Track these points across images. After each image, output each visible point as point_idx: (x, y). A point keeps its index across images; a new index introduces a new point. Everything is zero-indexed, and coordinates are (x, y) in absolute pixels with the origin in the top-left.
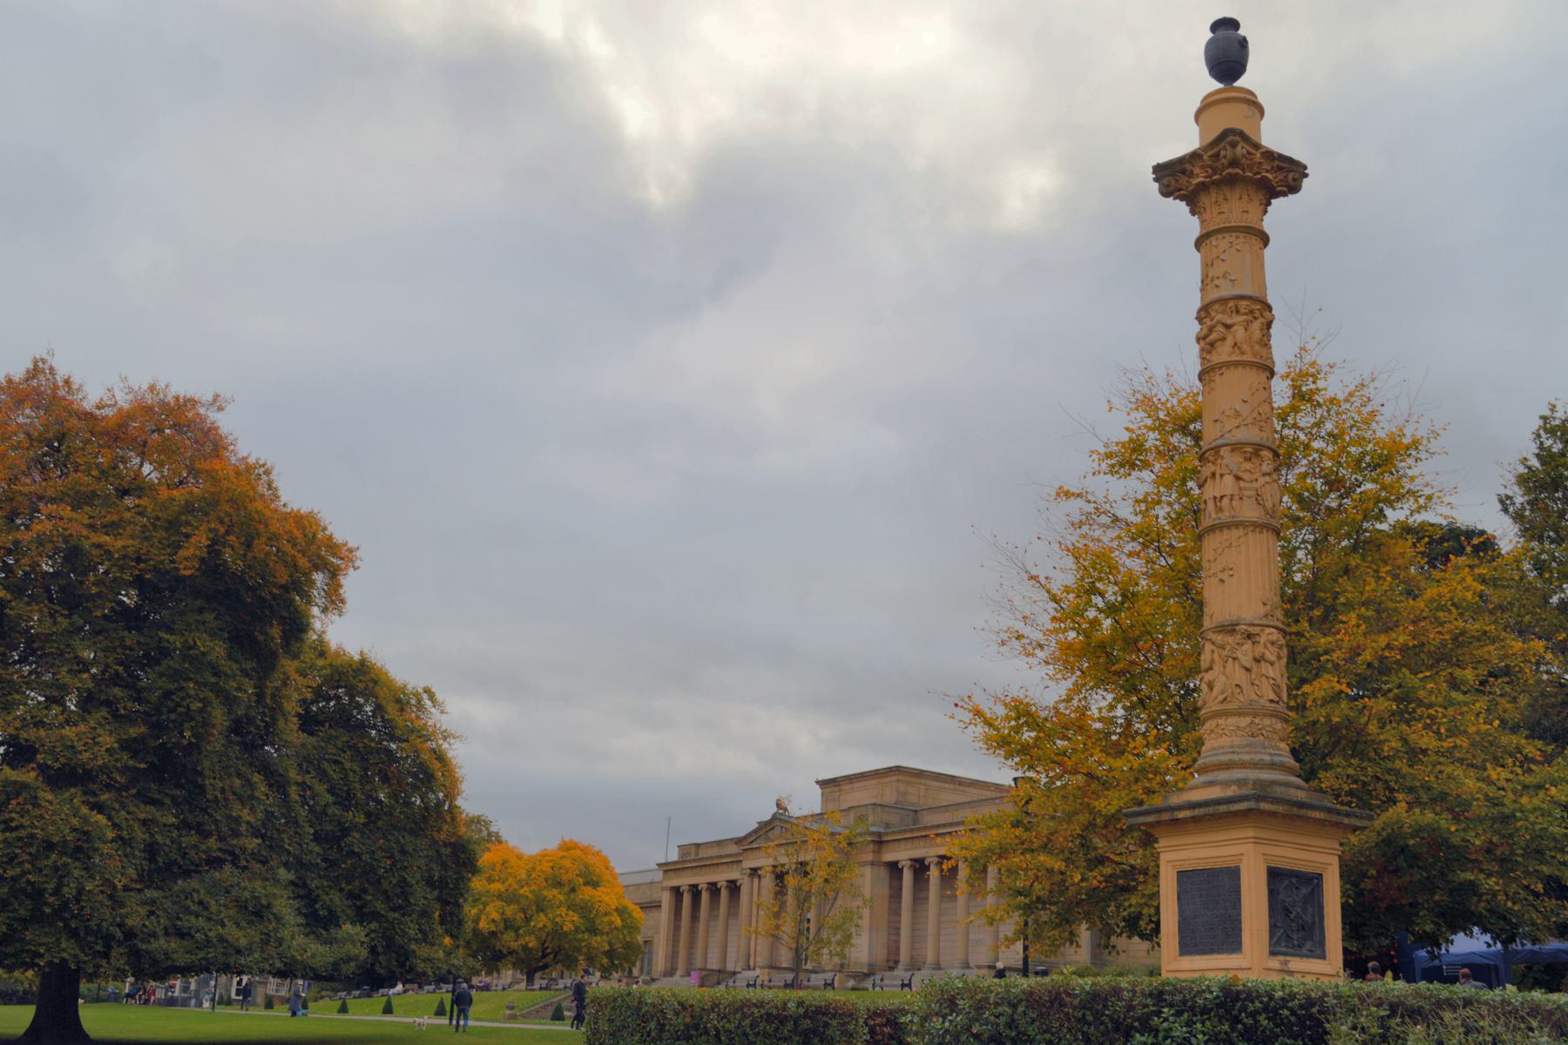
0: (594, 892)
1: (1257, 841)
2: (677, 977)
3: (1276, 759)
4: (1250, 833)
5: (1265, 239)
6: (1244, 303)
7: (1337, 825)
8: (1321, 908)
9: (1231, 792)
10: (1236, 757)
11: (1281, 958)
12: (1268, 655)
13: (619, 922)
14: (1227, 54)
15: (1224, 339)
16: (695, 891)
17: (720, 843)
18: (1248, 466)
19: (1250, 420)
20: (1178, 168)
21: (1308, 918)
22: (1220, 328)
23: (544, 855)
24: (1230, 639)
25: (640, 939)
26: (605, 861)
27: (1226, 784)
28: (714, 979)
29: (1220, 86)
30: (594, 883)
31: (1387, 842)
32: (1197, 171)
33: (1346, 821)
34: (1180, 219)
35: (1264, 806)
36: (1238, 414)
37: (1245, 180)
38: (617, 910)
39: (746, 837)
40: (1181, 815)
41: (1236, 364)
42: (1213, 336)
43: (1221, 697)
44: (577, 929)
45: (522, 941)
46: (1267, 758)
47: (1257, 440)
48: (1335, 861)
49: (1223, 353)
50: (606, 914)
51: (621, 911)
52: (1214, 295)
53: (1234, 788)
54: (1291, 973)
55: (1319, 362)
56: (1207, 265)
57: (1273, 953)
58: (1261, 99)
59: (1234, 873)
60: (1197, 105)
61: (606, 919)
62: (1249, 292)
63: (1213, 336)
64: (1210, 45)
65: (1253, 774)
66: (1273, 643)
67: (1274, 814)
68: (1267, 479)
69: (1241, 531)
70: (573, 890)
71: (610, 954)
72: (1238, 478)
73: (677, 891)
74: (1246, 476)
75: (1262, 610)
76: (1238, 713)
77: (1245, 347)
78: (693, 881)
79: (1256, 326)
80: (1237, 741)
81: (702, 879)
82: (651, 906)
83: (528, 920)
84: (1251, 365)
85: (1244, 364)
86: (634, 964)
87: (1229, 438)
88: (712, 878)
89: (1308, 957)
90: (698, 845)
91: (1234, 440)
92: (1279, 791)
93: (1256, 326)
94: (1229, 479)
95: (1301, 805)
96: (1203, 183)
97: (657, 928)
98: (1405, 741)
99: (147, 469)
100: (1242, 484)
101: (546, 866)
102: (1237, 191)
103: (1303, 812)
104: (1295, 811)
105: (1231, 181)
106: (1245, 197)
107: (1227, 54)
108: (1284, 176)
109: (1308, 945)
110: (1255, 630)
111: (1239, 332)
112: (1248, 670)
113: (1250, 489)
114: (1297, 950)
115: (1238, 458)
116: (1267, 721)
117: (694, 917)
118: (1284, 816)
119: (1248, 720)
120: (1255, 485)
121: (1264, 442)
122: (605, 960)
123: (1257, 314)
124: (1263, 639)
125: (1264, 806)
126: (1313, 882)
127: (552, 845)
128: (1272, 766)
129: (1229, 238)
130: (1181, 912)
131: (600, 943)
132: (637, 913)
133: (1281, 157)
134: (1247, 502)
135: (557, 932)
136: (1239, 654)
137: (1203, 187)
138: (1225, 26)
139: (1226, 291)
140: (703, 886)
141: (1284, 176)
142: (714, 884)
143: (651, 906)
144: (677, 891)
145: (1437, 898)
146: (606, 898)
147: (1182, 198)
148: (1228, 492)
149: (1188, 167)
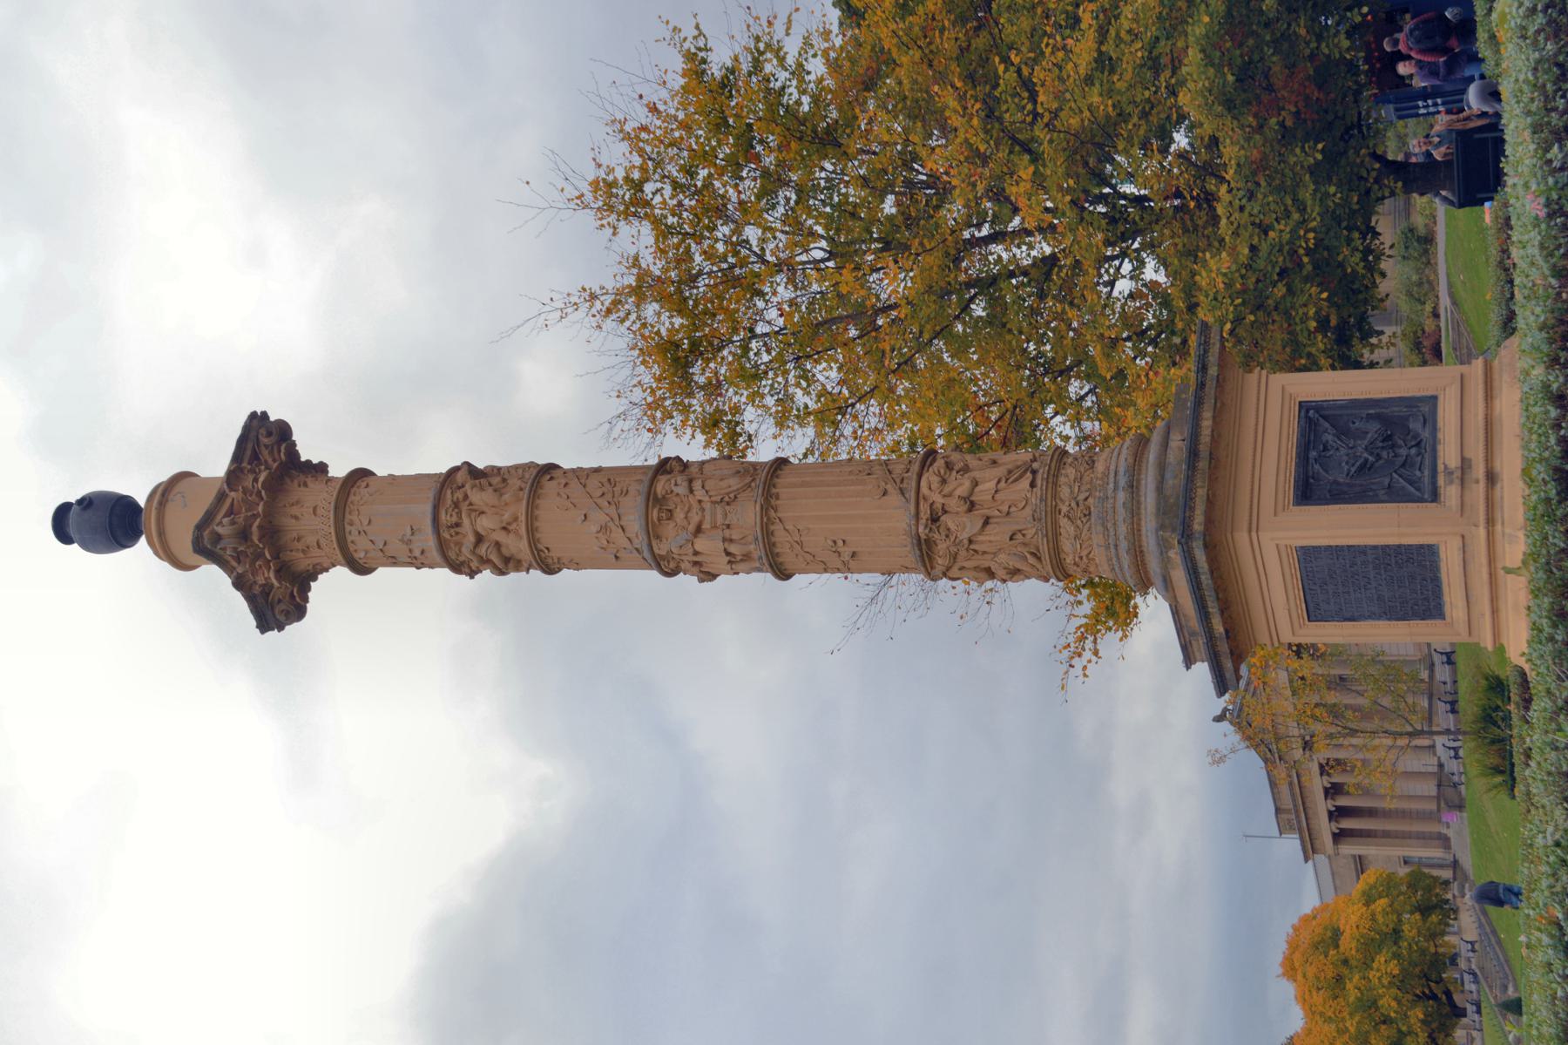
0: (1347, 934)
1: (1254, 527)
2: (1450, 833)
3: (1122, 481)
4: (1242, 538)
5: (360, 475)
6: (443, 516)
7: (1220, 382)
8: (1355, 404)
9: (1175, 555)
10: (1124, 545)
11: (1441, 481)
12: (963, 490)
13: (1383, 902)
14: (101, 522)
15: (498, 545)
16: (1338, 813)
17: (1273, 785)
18: (679, 515)
19: (612, 511)
20: (260, 600)
21: (1374, 428)
22: (482, 550)
23: (1303, 1000)
24: (942, 547)
25: (1403, 871)
26: (1306, 920)
27: (1166, 563)
28: (1449, 791)
29: (143, 539)
30: (1337, 934)
31: (1229, 105)
32: (261, 580)
33: (1213, 371)
34: (333, 589)
35: (1198, 525)
36: (604, 529)
37: (269, 514)
38: (1367, 904)
39: (1266, 761)
40: (1219, 627)
41: (532, 531)
42: (494, 558)
43: (1031, 560)
44: (1396, 956)
45: (1417, 1027)
46: (1122, 496)
47: (641, 500)
49: (517, 545)
50: (1373, 919)
51: (1368, 899)
52: (435, 554)
53: (1172, 554)
54: (1465, 464)
55: (591, 178)
56: (394, 562)
57: (1435, 497)
58: (164, 476)
59: (1308, 555)
60: (166, 565)
61: (1380, 919)
62: (428, 508)
63: (494, 558)
64: (87, 546)
65: (1149, 523)
66: (944, 481)
67: (1210, 502)
68: (697, 485)
69: (777, 527)
70: (1346, 962)
71: (1425, 910)
72: (698, 530)
73: (1339, 836)
74: (695, 519)
75: (894, 498)
76: (1055, 536)
77: (507, 517)
78: (1324, 817)
79: (477, 497)
80: (1097, 539)
81: (1321, 807)
82: (1361, 864)
83: (1386, 1021)
84: (532, 506)
85: (531, 518)
86: (1436, 879)
87: (641, 541)
88: (1319, 794)
89: (1435, 429)
90: (1278, 811)
91: (643, 537)
92: (1174, 482)
93: (477, 497)
94: (701, 544)
95: (1193, 454)
96: (278, 572)
97: (1385, 857)
98: (1089, 80)
99: (938, 431)
100: (706, 526)
101: (1318, 998)
102: (288, 522)
104: (1203, 464)
105: (272, 533)
106: (295, 510)
107: (101, 522)
108: (265, 442)
109: (1415, 425)
110: (925, 513)
111: (484, 524)
112: (987, 522)
113: (714, 515)
114: (1426, 447)
115: (669, 529)
116: (1065, 492)
117: (1371, 813)
118: (1213, 480)
119: (1064, 522)
120: (707, 506)
121: (644, 488)
122: (1434, 918)
123: (459, 495)
124: (938, 500)
125: (1198, 525)
126: (1314, 417)
127: (1288, 989)
128: (1133, 487)
129: (352, 536)
130: (1372, 616)
131: (1411, 924)
132: (1370, 877)
133: (237, 457)
134: (732, 519)
135: (1401, 982)
136: (964, 536)
137: (284, 570)
138: (65, 523)
139: (431, 543)
140: (1330, 805)
141: (265, 442)
142: (1327, 791)
143: (1361, 864)
144: (1339, 836)
145: (1303, 32)
146: (1352, 920)
147: (305, 590)
148: (721, 546)
149: (257, 590)
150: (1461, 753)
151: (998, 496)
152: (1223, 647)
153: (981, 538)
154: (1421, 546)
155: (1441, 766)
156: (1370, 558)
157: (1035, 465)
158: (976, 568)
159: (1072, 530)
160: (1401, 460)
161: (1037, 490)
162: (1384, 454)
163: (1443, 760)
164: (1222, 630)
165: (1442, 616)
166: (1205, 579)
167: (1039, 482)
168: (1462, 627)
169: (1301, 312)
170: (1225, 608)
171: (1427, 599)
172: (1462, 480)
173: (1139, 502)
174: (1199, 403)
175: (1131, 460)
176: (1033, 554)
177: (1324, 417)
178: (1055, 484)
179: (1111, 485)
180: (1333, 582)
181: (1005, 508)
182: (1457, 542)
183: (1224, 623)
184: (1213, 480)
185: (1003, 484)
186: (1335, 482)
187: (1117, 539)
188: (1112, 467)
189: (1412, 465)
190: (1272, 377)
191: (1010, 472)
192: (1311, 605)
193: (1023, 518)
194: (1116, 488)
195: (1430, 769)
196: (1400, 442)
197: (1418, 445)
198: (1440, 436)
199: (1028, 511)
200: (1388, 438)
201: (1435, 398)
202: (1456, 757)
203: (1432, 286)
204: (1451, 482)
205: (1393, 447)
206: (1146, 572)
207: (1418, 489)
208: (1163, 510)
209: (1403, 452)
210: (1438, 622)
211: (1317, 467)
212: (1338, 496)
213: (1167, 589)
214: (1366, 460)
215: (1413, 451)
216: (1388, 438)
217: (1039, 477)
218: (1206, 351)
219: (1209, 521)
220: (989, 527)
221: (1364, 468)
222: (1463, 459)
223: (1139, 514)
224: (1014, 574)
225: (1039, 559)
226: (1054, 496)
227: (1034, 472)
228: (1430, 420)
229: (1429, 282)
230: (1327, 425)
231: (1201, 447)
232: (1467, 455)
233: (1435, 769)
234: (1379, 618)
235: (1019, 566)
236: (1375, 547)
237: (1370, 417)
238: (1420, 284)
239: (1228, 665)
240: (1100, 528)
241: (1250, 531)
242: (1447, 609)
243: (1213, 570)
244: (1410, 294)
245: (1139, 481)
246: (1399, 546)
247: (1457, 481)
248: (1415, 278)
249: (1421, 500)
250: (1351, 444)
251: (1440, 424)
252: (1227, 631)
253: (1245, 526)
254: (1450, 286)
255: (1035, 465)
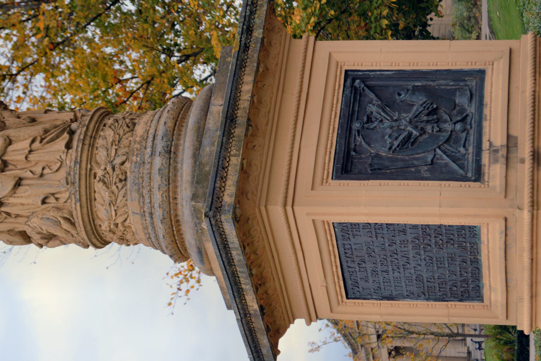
1: (290, 201)
3: (160, 145)
4: (276, 211)
7: (265, 46)
10: (158, 213)
11: (485, 158)
21: (419, 101)
33: (258, 33)
35: (228, 197)
40: (253, 305)
43: (66, 225)
46: (158, 161)
48: (326, 47)
54: (511, 142)
57: (478, 175)
59: (345, 232)
65: (185, 191)
67: (244, 172)
80: (133, 206)
89: (481, 105)
92: (210, 149)
95: (230, 119)
103: (241, 115)
104: (239, 131)
109: (461, 100)
112: (19, 183)
114: (471, 123)
116: (101, 155)
118: (249, 146)
119: (98, 186)
125: (228, 197)
126: (358, 86)
128: (171, 152)
150: (483, 346)
151: (31, 157)
152: (259, 324)
153: (12, 200)
154: (463, 227)
155: (469, 353)
156: (410, 237)
157: (74, 126)
158: (10, 232)
159: (106, 195)
160: (446, 135)
161: (72, 152)
162: (429, 129)
163: (471, 349)
164: (256, 307)
165: (479, 297)
166: (237, 255)
167: (75, 143)
168: (500, 311)
169: (375, 12)
170: (259, 284)
171: (465, 281)
172: (507, 159)
173: (175, 169)
174: (240, 65)
175: (170, 124)
176: (65, 219)
177: (369, 88)
178: (92, 146)
179: (149, 150)
180: (368, 261)
181: (38, 170)
182: (498, 227)
183: (259, 299)
184: (249, 146)
185: (37, 144)
186: (377, 156)
187: (152, 207)
188: (152, 131)
189: (457, 141)
190: (319, 43)
191: (46, 131)
192: (349, 283)
193: (56, 181)
194: (152, 154)
195: (462, 355)
196: (446, 117)
197: (464, 120)
198: (486, 111)
199: (62, 173)
200: (434, 112)
201: (482, 73)
202: (480, 348)
203: (477, 22)
204: (496, 161)
205: (438, 121)
206: (183, 243)
207: (462, 167)
208: (198, 179)
209: (448, 127)
210: (476, 304)
211: (359, 139)
212: (378, 171)
213: (202, 261)
214: (410, 134)
215: (458, 126)
216: (434, 112)
217: (76, 137)
218: (252, 13)
219: (241, 193)
220: (21, 189)
221: (408, 142)
222: (508, 136)
223: (175, 181)
224: (49, 239)
225: (73, 224)
226: (91, 158)
227: (72, 133)
228: (477, 95)
229: (476, 19)
230: (372, 95)
231: (240, 113)
232: (513, 133)
233: (466, 355)
234: (418, 297)
235: (53, 231)
236: (415, 227)
237: (415, 89)
238: (469, 18)
239: (264, 341)
240: (135, 195)
241: (285, 205)
242: (486, 292)
243: (246, 243)
244: (462, 26)
245: (177, 146)
246: (440, 226)
247: (503, 160)
248: (465, 14)
249: (464, 179)
250: (396, 116)
251: (487, 99)
252: (262, 308)
253: (280, 199)
254: (490, 19)
255: (74, 126)
